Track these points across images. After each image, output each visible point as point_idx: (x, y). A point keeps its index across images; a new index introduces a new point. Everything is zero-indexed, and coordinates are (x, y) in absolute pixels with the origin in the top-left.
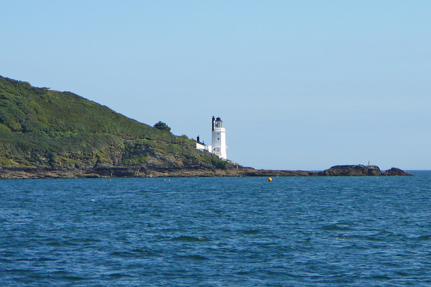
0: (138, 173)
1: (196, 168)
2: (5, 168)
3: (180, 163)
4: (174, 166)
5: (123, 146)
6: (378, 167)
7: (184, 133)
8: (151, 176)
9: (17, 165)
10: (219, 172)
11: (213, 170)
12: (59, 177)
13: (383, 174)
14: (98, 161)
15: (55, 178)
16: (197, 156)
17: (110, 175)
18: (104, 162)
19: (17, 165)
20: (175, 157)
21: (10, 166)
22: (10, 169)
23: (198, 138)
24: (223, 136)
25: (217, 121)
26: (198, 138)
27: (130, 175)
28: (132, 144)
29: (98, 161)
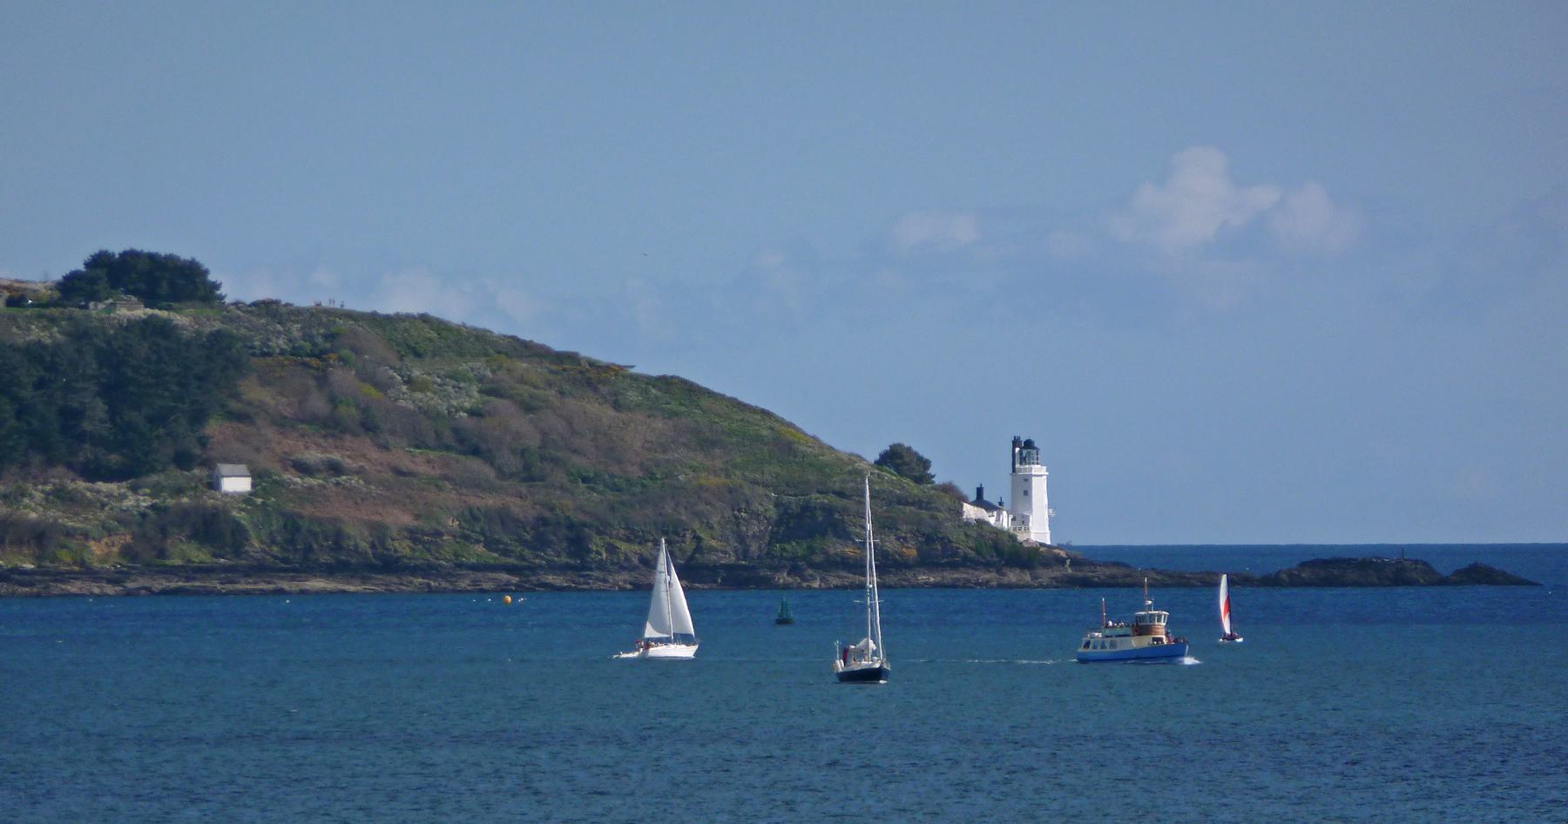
0: (783, 578)
1: (953, 566)
2: (460, 566)
3: (911, 552)
4: (895, 560)
5: (773, 513)
6: (1425, 564)
7: (94, 249)
8: (816, 585)
9: (493, 557)
10: (1012, 576)
11: (999, 571)
12: (569, 588)
13: (1443, 582)
14: (698, 549)
15: (561, 589)
16: (956, 537)
17: (715, 582)
18: (712, 549)
19: (493, 557)
20: (898, 539)
21: (473, 560)
22: (474, 568)
23: (980, 491)
24: (1040, 489)
25: (1025, 449)
26: (980, 491)
27: (765, 583)
28: (795, 509)
29: (698, 549)
